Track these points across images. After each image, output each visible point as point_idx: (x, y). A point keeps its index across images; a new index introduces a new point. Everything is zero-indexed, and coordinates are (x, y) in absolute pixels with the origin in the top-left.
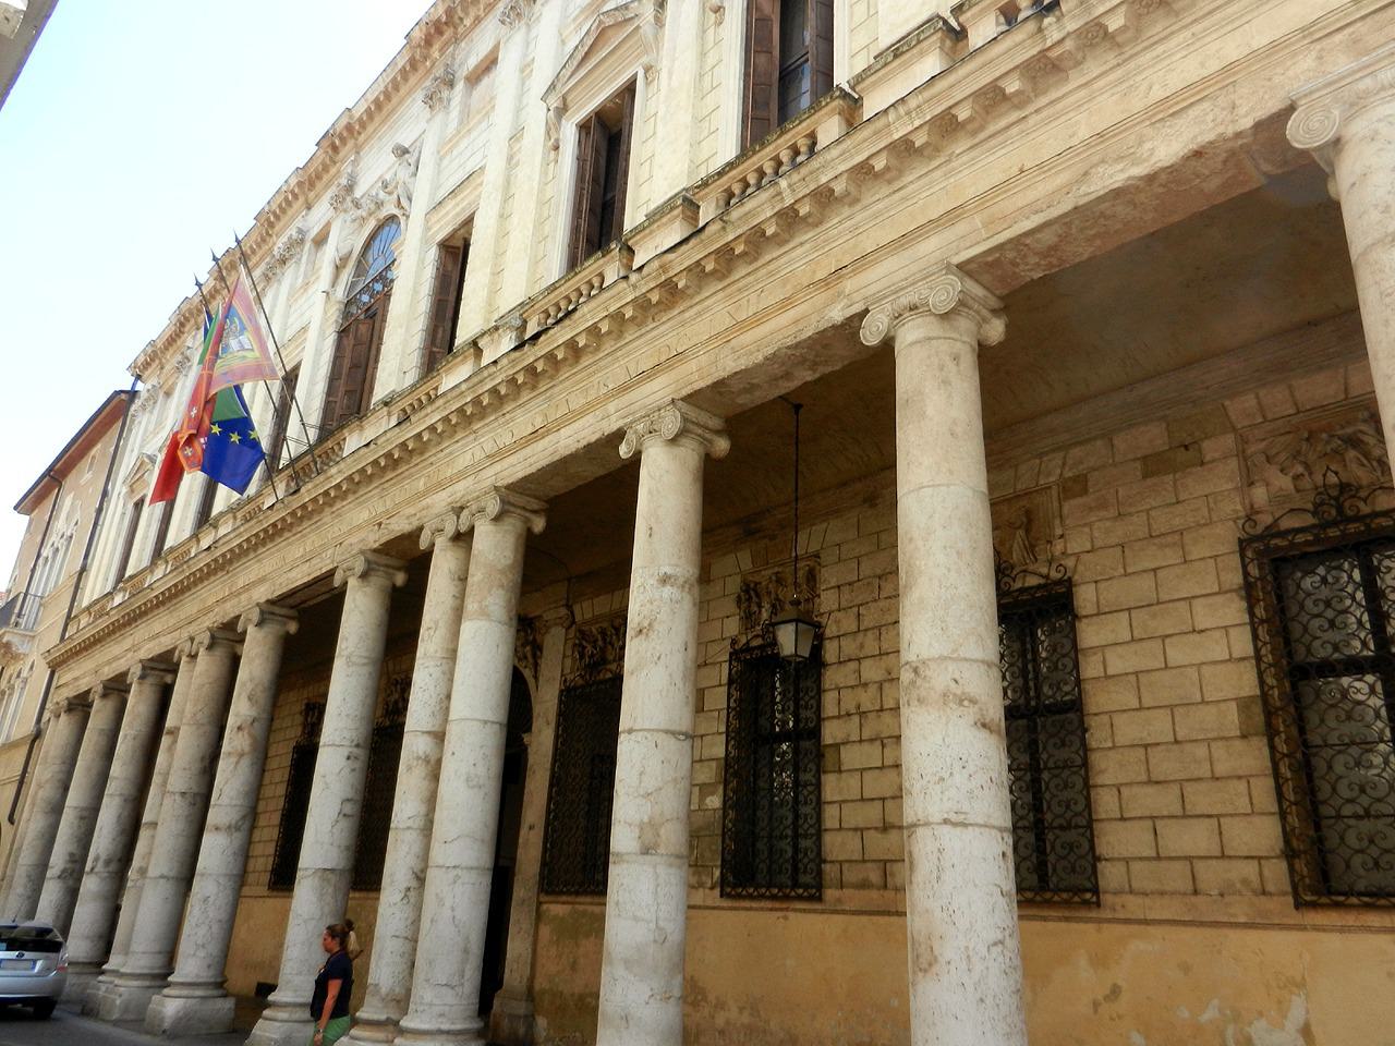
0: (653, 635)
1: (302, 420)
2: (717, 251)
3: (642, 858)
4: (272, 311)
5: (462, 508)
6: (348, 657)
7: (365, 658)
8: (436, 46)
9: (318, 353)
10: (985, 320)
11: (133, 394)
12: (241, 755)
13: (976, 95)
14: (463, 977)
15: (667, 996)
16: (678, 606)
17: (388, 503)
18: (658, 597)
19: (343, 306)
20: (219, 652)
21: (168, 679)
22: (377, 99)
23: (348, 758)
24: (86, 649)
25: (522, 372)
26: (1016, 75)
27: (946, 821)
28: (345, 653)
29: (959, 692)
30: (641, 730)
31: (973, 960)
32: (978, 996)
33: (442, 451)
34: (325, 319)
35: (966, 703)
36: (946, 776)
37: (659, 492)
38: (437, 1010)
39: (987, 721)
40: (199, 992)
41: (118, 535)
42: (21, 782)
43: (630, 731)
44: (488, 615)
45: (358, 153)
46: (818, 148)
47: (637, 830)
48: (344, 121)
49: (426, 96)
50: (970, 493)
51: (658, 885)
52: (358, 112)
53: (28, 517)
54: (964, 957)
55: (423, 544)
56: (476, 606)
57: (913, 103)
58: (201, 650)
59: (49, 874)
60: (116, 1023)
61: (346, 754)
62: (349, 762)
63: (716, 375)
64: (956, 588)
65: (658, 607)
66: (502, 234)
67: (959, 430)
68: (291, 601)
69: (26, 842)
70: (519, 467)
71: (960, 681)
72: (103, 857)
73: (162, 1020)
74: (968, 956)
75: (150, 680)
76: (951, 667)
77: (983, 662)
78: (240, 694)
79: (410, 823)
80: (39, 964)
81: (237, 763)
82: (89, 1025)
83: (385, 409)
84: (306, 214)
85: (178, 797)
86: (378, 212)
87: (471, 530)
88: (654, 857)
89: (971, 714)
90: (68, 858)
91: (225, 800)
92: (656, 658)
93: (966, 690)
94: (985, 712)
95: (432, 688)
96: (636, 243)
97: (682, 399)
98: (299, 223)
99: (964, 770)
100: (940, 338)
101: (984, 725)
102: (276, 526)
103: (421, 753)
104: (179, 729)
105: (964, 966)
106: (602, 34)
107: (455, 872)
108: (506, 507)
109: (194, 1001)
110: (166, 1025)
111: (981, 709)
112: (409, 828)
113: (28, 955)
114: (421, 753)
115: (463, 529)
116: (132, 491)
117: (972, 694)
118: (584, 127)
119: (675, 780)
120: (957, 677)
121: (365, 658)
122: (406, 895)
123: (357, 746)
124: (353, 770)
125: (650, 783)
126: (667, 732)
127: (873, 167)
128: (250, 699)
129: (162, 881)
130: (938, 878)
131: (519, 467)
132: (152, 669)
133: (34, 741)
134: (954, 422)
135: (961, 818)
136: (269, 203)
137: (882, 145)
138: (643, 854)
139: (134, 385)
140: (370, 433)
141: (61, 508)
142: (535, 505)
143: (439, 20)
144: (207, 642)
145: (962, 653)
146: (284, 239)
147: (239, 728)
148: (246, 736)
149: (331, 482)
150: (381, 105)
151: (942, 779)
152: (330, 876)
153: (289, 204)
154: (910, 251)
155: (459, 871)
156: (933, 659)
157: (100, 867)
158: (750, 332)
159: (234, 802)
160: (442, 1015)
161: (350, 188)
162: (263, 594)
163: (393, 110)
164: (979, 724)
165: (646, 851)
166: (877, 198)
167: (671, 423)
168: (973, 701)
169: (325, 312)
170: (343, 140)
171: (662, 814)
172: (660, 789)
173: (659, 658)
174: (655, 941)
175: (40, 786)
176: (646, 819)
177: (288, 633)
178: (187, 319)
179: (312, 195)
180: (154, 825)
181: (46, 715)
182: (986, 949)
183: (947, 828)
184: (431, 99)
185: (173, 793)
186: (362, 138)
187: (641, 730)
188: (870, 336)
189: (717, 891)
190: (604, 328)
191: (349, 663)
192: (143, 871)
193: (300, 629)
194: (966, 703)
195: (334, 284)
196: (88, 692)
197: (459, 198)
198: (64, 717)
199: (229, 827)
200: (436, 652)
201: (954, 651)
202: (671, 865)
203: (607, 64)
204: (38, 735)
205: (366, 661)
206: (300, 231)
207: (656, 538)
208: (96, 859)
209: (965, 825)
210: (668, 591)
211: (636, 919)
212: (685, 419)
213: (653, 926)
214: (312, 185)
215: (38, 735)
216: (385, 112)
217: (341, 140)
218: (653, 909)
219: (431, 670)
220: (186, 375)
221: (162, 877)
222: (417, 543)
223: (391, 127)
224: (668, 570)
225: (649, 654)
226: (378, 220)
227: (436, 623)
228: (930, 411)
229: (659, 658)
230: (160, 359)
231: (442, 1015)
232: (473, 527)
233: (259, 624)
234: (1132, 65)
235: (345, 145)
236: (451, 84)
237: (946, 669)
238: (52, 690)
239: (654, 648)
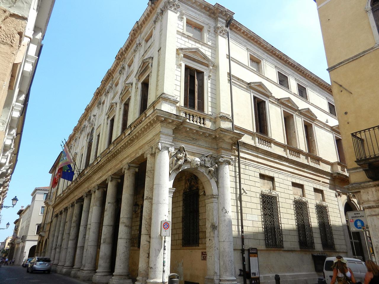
8: (99, 96)
9: (85, 152)
12: (74, 227)
20: (101, 190)
21: (82, 203)
23: (84, 228)
24: (57, 205)
38: (88, 267)
41: (63, 181)
42: (49, 231)
48: (88, 107)
53: (52, 174)
58: (96, 190)
60: (59, 274)
66: (102, 139)
67: (128, 186)
75: (78, 204)
80: (47, 264)
82: (56, 274)
89: (124, 225)
91: (72, 235)
101: (126, 226)
102: (142, 130)
107: (91, 246)
108: (99, 188)
110: (64, 273)
113: (45, 263)
119: (109, 232)
125: (105, 233)
126: (108, 225)
128: (75, 217)
129: (65, 249)
132: (101, 187)
133: (51, 223)
134: (128, 185)
135: (121, 238)
142: (119, 177)
144: (97, 188)
145: (124, 217)
147: (74, 222)
153: (83, 120)
155: (91, 246)
162: (128, 160)
171: (106, 237)
177: (136, 172)
178: (71, 138)
179: (86, 118)
181: (53, 218)
186: (91, 109)
189: (137, 248)
191: (84, 212)
193: (139, 170)
195: (87, 139)
196: (106, 180)
198: (55, 218)
199: (73, 239)
202: (107, 244)
204: (52, 222)
206: (84, 125)
210: (109, 204)
214: (86, 117)
215: (52, 222)
220: (140, 51)
222: (143, 157)
224: (109, 201)
231: (89, 267)
233: (98, 189)
234: (139, 140)
235: (129, 47)
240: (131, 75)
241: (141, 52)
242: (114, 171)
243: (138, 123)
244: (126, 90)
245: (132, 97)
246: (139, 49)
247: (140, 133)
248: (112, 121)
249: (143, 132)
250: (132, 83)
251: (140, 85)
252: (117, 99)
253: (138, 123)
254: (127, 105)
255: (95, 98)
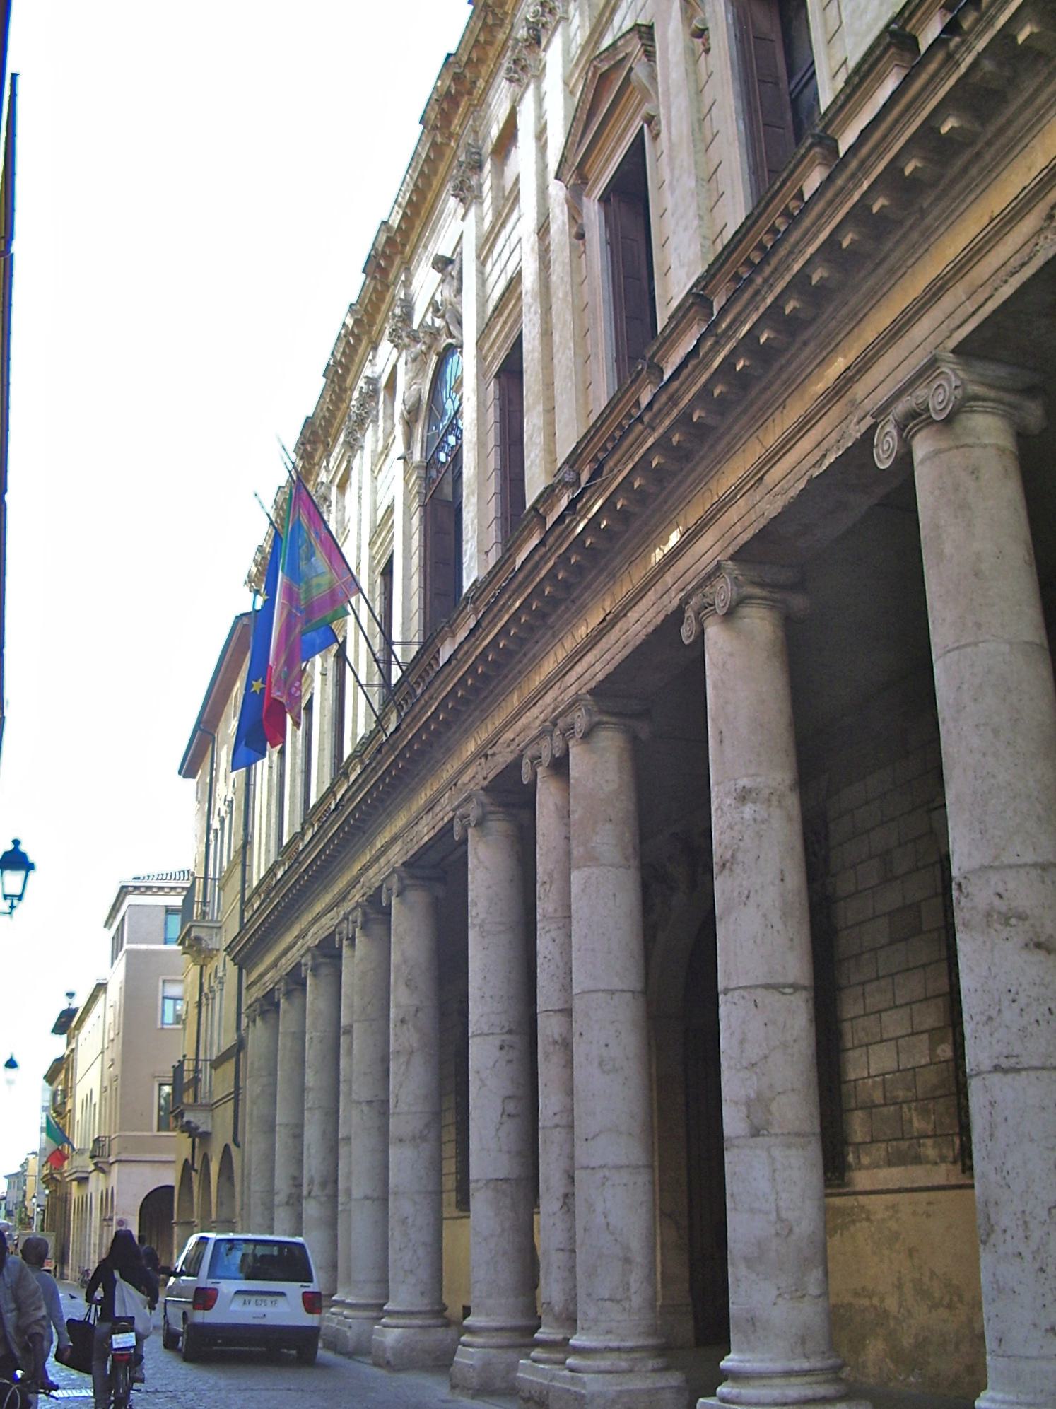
0: (738, 869)
3: (752, 1141)
4: (357, 664)
6: (481, 926)
7: (500, 923)
14: (628, 1289)
15: (799, 1294)
16: (764, 827)
18: (739, 819)
19: (422, 472)
23: (501, 1048)
27: (997, 1068)
28: (477, 921)
29: (1004, 909)
30: (735, 989)
31: (1031, 1226)
32: (1037, 1266)
34: (407, 492)
35: (1013, 921)
36: (994, 1013)
37: (724, 683)
39: (1042, 939)
40: (417, 1321)
43: (726, 991)
44: (597, 859)
45: (408, 269)
47: (744, 1109)
48: (383, 238)
49: (455, 188)
50: (1005, 648)
51: (774, 1171)
52: (395, 221)
54: (1020, 1222)
56: (581, 849)
59: (277, 1199)
61: (498, 1043)
62: (503, 1052)
64: (994, 776)
65: (740, 832)
69: (253, 1167)
70: (598, 667)
71: (1005, 895)
72: (317, 1179)
73: (385, 1350)
74: (1025, 1222)
76: (994, 878)
77: (1034, 865)
78: (396, 982)
79: (557, 1120)
81: (408, 1063)
84: (374, 357)
85: (365, 1108)
88: (767, 1139)
90: (291, 1182)
92: (744, 898)
93: (1014, 904)
94: (1038, 930)
95: (557, 957)
96: (663, 358)
97: (732, 558)
98: (368, 371)
99: (1014, 1005)
100: (950, 449)
101: (1038, 945)
103: (557, 1037)
104: (351, 1026)
105: (1021, 1234)
106: (603, 80)
109: (412, 1331)
111: (1032, 926)
112: (557, 1126)
114: (557, 1037)
117: (1021, 909)
118: (604, 200)
120: (1000, 890)
121: (500, 923)
122: (565, 1203)
123: (510, 1032)
124: (510, 1062)
129: (368, 1202)
130: (991, 1135)
131: (598, 667)
135: (1013, 1061)
136: (333, 354)
138: (753, 1136)
141: (218, 765)
143: (448, 92)
146: (356, 395)
147: (403, 1021)
148: (412, 1030)
150: (417, 210)
151: (990, 1018)
152: (504, 1186)
154: (906, 338)
156: (973, 872)
157: (316, 1190)
158: (810, 433)
159: (413, 1109)
160: (609, 1332)
161: (407, 316)
164: (1031, 945)
165: (756, 1132)
168: (1022, 917)
169: (406, 483)
170: (390, 259)
171: (771, 1087)
172: (766, 1057)
173: (748, 897)
174: (777, 1234)
175: (253, 1102)
176: (753, 1095)
180: (348, 1139)
181: (244, 1021)
182: (1046, 1212)
183: (997, 1077)
184: (461, 190)
185: (359, 1103)
187: (735, 989)
192: (348, 1192)
194: (1013, 921)
199: (414, 1138)
200: (556, 910)
201: (996, 857)
202: (789, 1146)
205: (502, 928)
207: (726, 742)
208: (311, 1182)
209: (1018, 1071)
211: (752, 1211)
213: (773, 1217)
217: (390, 256)
218: (772, 1198)
219: (554, 934)
221: (366, 1198)
223: (433, 231)
225: (736, 894)
227: (550, 875)
228: (948, 549)
229: (748, 897)
236: (479, 167)
237: (988, 881)
238: (244, 991)
239: (741, 886)
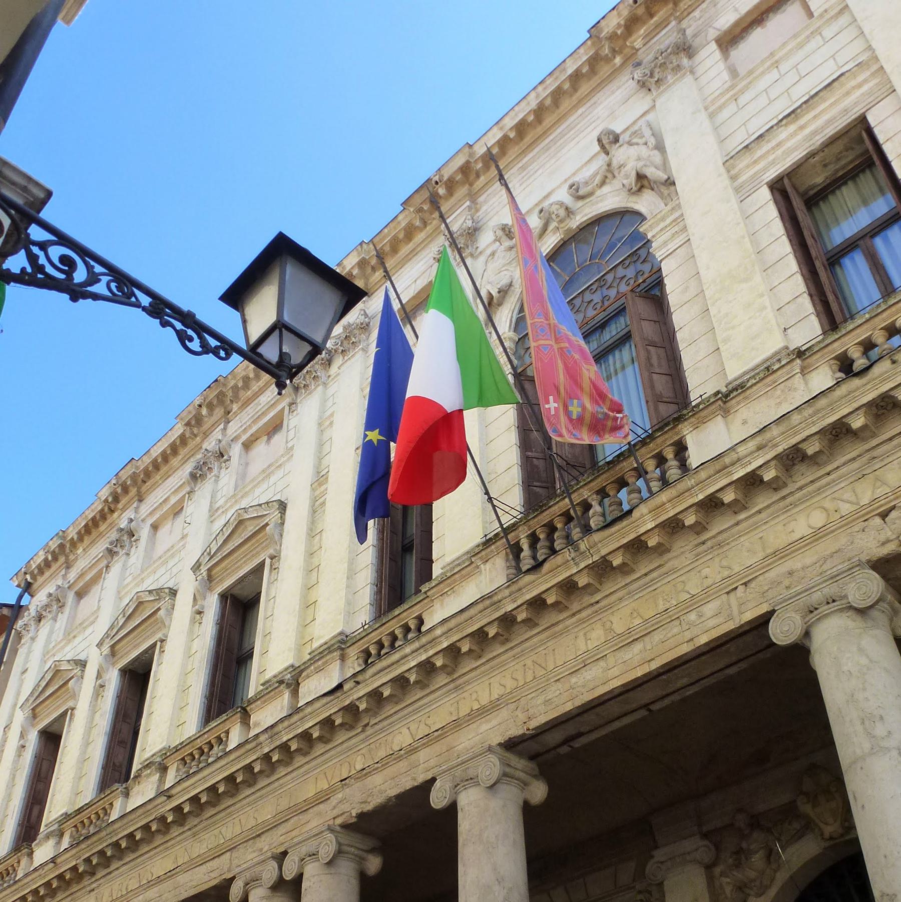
1: (487, 493)
2: (471, 635)
5: (285, 854)
10: (526, 784)
11: (17, 609)
13: (419, 665)
17: (107, 894)
22: (164, 452)
25: (317, 727)
26: (861, 412)
33: (703, 543)
46: (424, 629)
48: (460, 161)
52: (613, 24)
55: (438, 799)
57: (796, 418)
63: (374, 802)
68: (534, 747)
83: (798, 361)
86: (568, 221)
87: (298, 880)
102: (39, 892)
115: (288, 875)
116: (34, 716)
127: (382, 694)
137: (814, 429)
139: (20, 597)
140: (136, 800)
149: (730, 474)
163: (545, 133)
166: (683, 550)
167: (328, 846)
170: (451, 185)
188: (438, 799)
190: (294, 746)
197: (802, 121)
203: (235, 555)
212: (339, 844)
216: (528, 139)
220: (128, 554)
226: (569, 230)
230: (67, 557)
232: (301, 875)
240: (272, 472)
241: (222, 483)
242: (384, 787)
243: (89, 818)
244: (58, 682)
245: (168, 647)
246: (215, 471)
247: (94, 863)
248: (51, 739)
249: (68, 883)
250: (86, 662)
251: (113, 679)
252: (89, 646)
253: (89, 818)
254: (137, 678)
255: (46, 560)
